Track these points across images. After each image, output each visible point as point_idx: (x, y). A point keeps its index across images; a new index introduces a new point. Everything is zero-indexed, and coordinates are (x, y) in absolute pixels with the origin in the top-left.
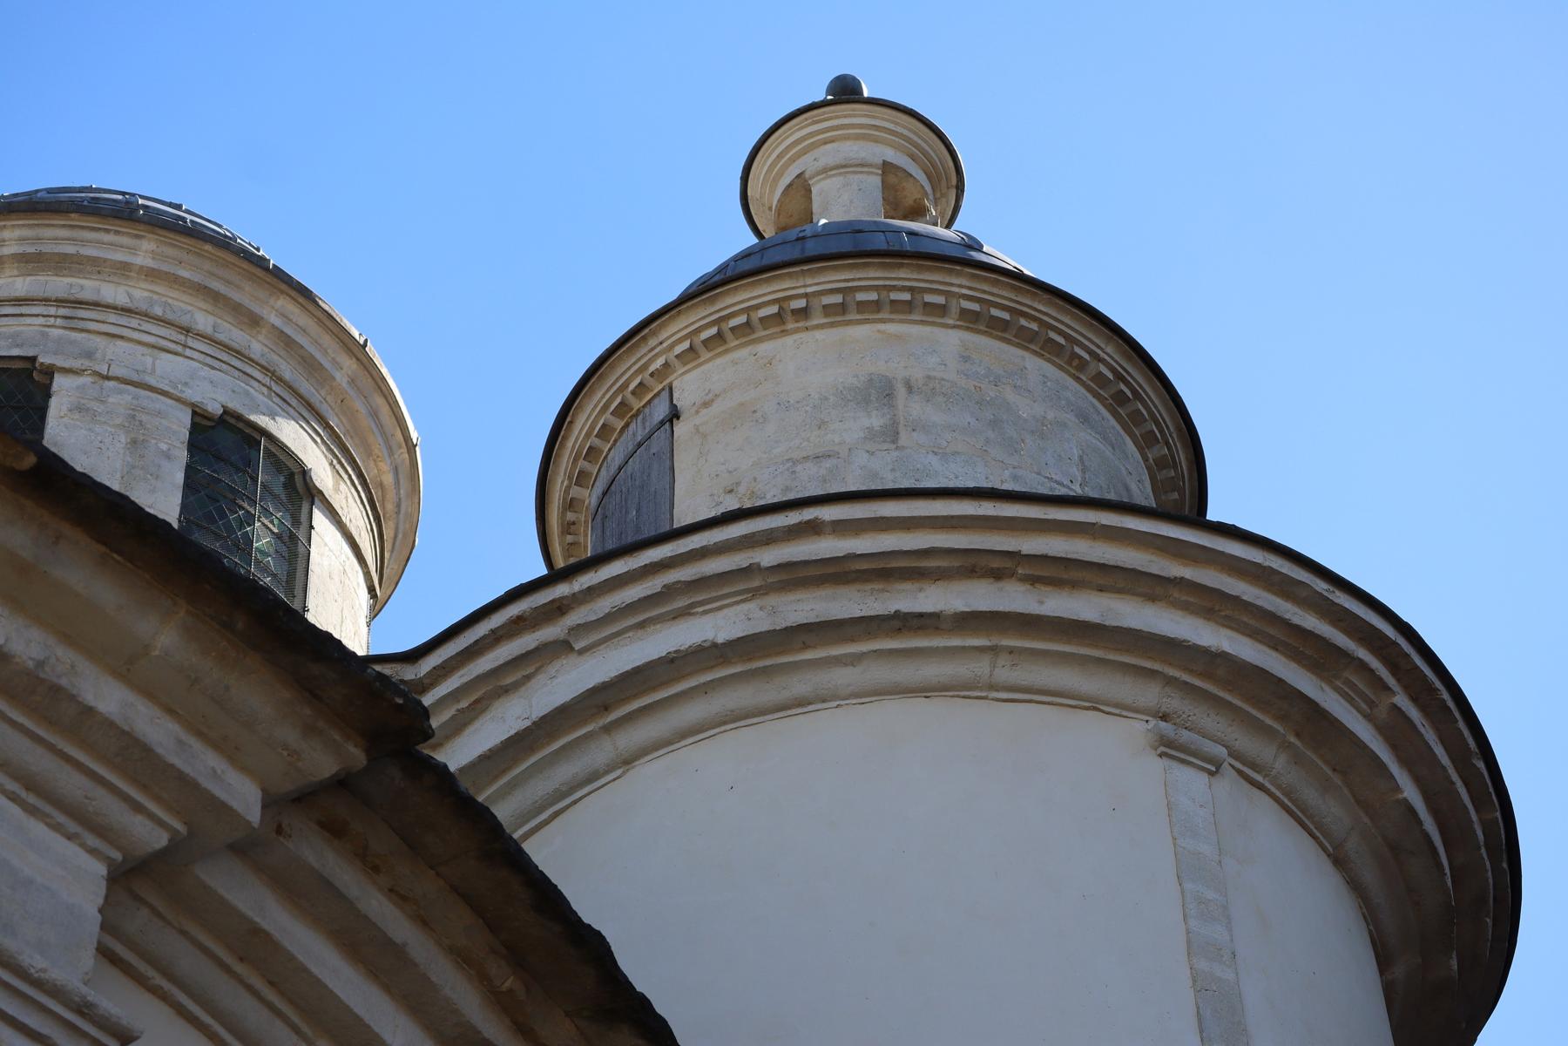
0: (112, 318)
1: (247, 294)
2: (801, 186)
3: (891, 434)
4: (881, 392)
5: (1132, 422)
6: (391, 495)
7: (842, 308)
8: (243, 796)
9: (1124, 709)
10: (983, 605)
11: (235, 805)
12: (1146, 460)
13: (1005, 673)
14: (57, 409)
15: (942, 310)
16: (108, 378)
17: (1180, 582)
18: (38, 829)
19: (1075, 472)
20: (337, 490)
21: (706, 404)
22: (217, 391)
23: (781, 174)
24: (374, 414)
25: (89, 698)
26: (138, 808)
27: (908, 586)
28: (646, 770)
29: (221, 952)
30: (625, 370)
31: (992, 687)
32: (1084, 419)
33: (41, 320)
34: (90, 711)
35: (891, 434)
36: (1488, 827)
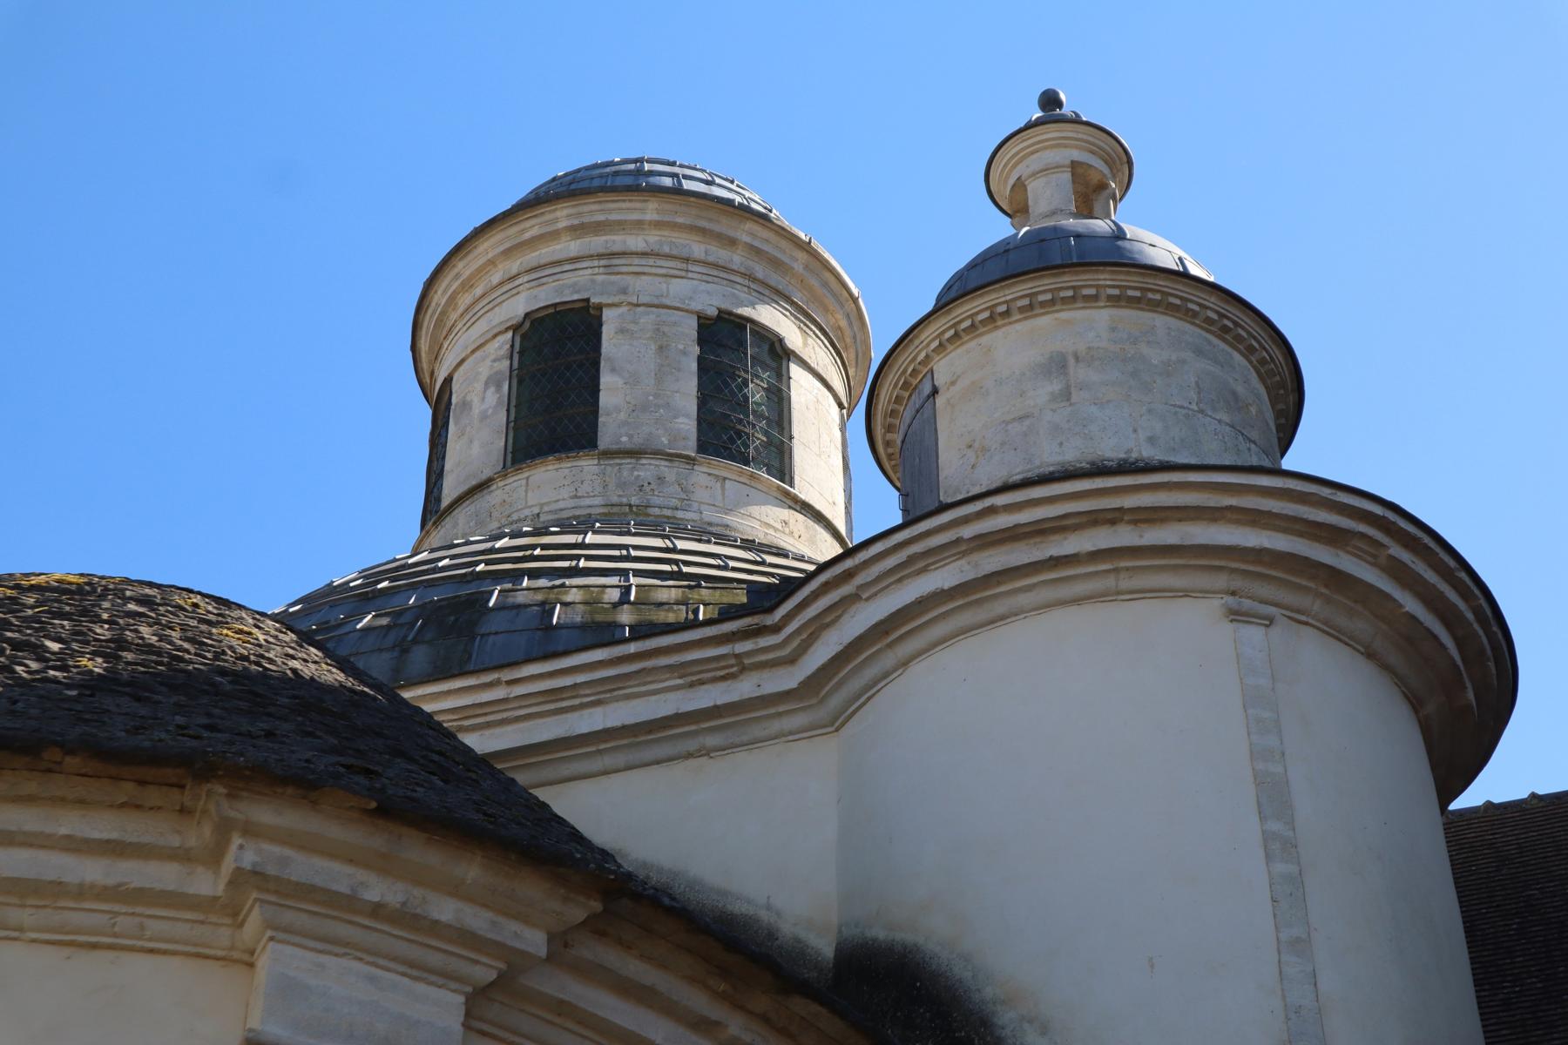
0: (636, 261)
1: (725, 226)
2: (1020, 186)
3: (1066, 395)
4: (1057, 365)
5: (1236, 342)
6: (848, 333)
7: (1031, 307)
8: (534, 941)
9: (1206, 593)
10: (1104, 545)
11: (530, 950)
12: (1251, 362)
13: (1126, 583)
14: (607, 332)
15: (1095, 298)
16: (638, 305)
17: (1230, 508)
18: (421, 988)
19: (1193, 395)
20: (805, 344)
21: (953, 383)
22: (711, 299)
23: (1007, 177)
24: (825, 284)
25: (435, 915)
26: (477, 962)
27: (1056, 537)
28: (917, 668)
29: (549, 1016)
30: (903, 361)
31: (1119, 593)
32: (1199, 352)
33: (589, 271)
34: (437, 922)
35: (1066, 395)
36: (1478, 612)
